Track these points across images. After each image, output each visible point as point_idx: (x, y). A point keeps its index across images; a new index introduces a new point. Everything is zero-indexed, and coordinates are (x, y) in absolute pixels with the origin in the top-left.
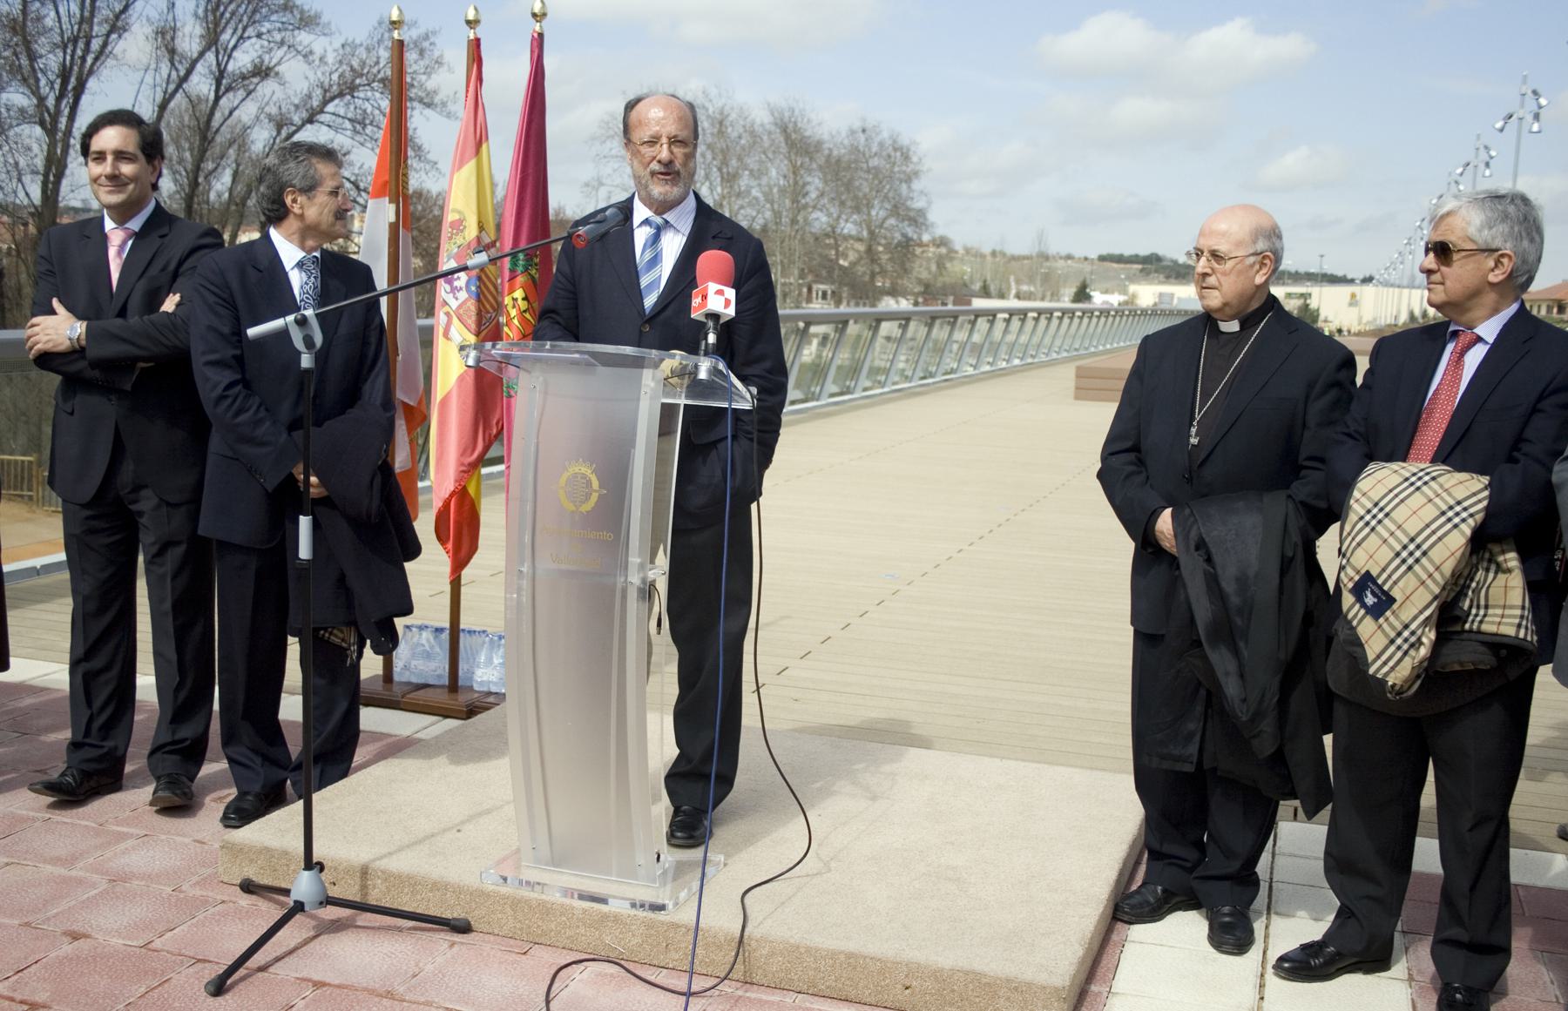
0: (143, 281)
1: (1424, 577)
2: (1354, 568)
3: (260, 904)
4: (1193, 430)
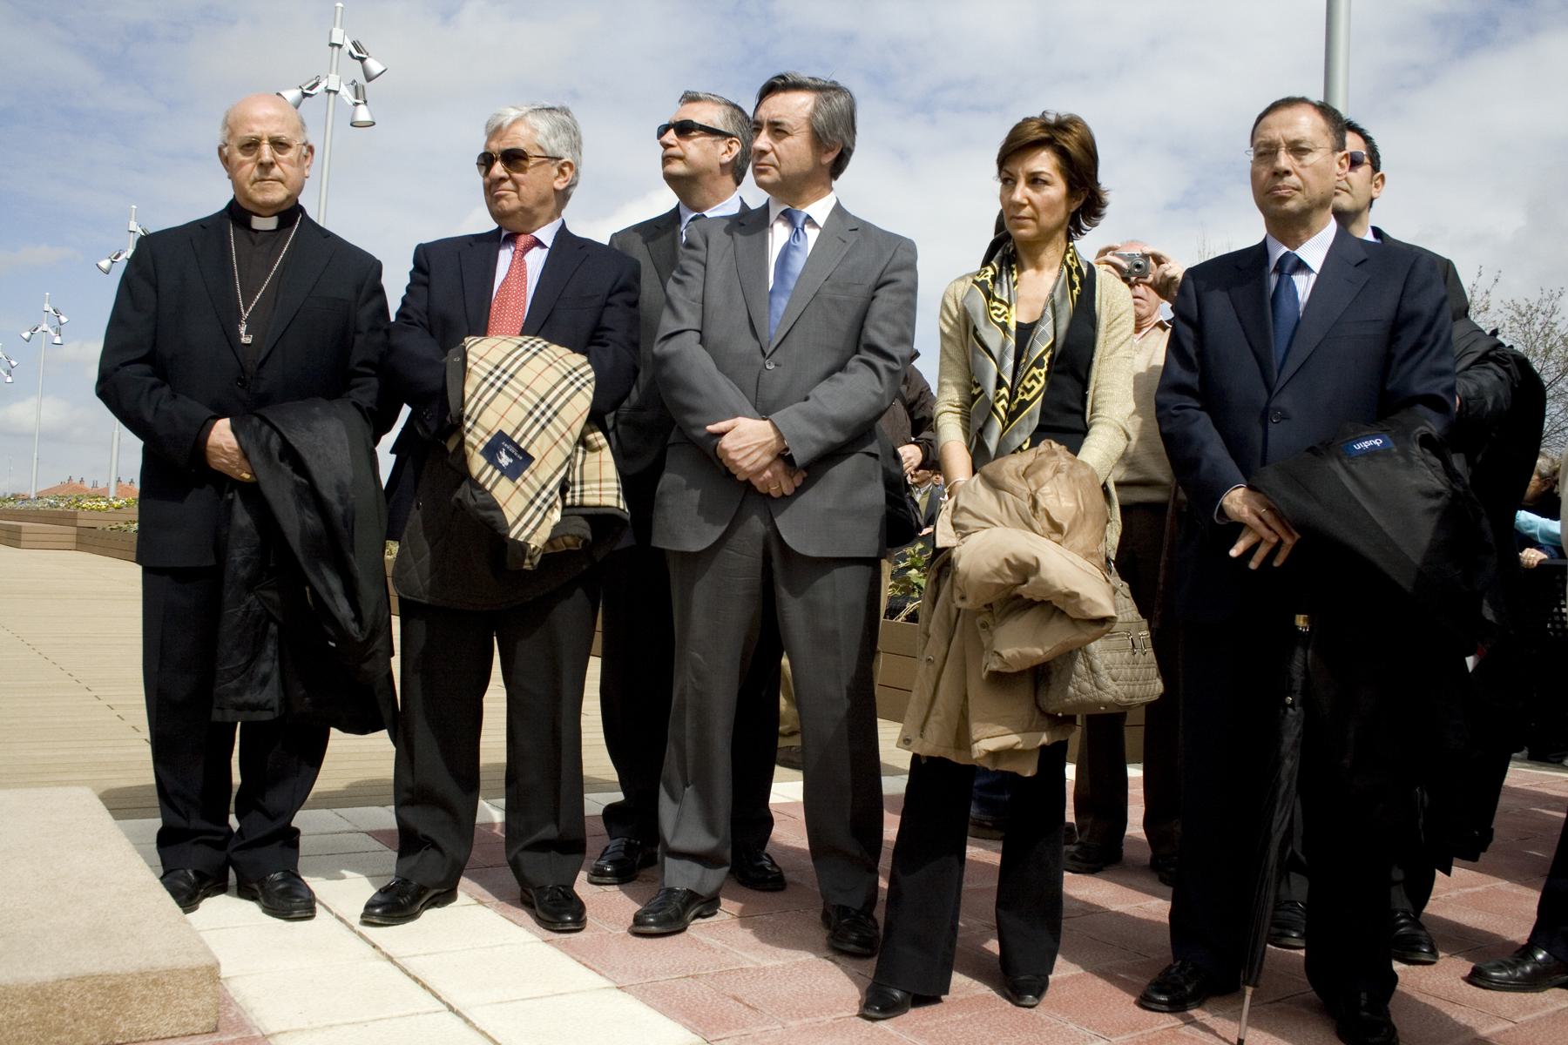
1: (557, 437)
2: (484, 429)
4: (243, 330)
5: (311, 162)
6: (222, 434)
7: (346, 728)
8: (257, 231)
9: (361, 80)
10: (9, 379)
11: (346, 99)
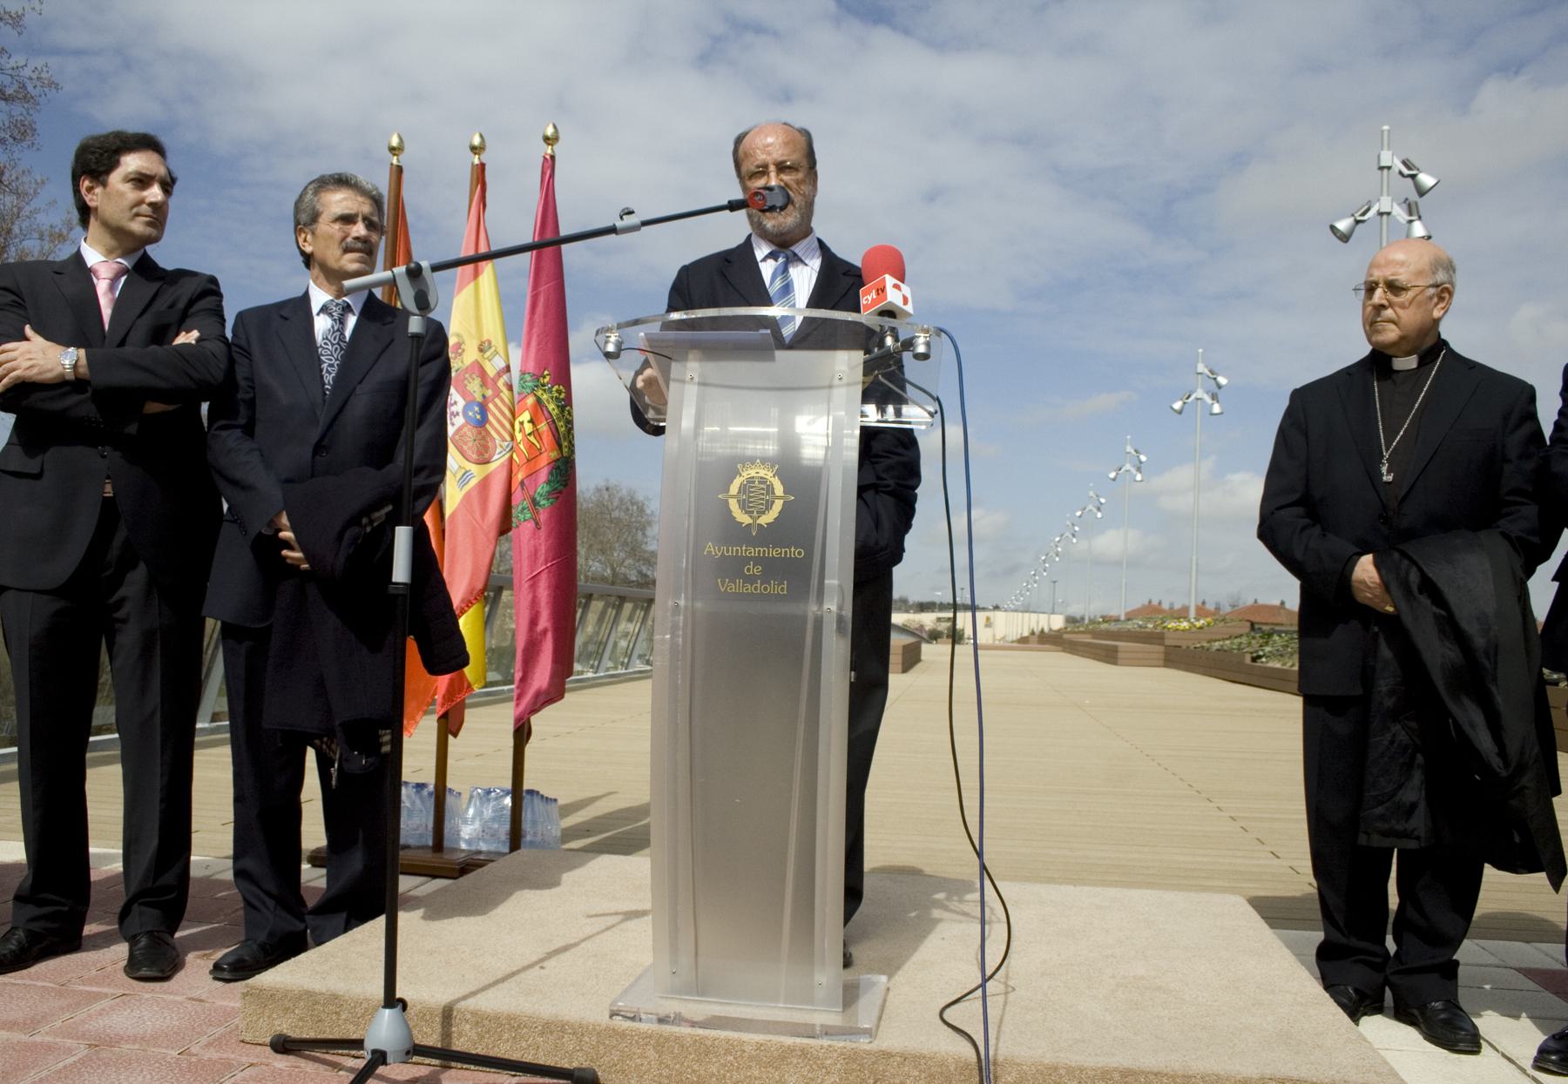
0: (148, 317)
3: (302, 1065)
4: (1384, 469)
6: (1365, 569)
7: (1500, 866)
9: (1414, 196)
10: (1099, 515)
11: (1398, 218)
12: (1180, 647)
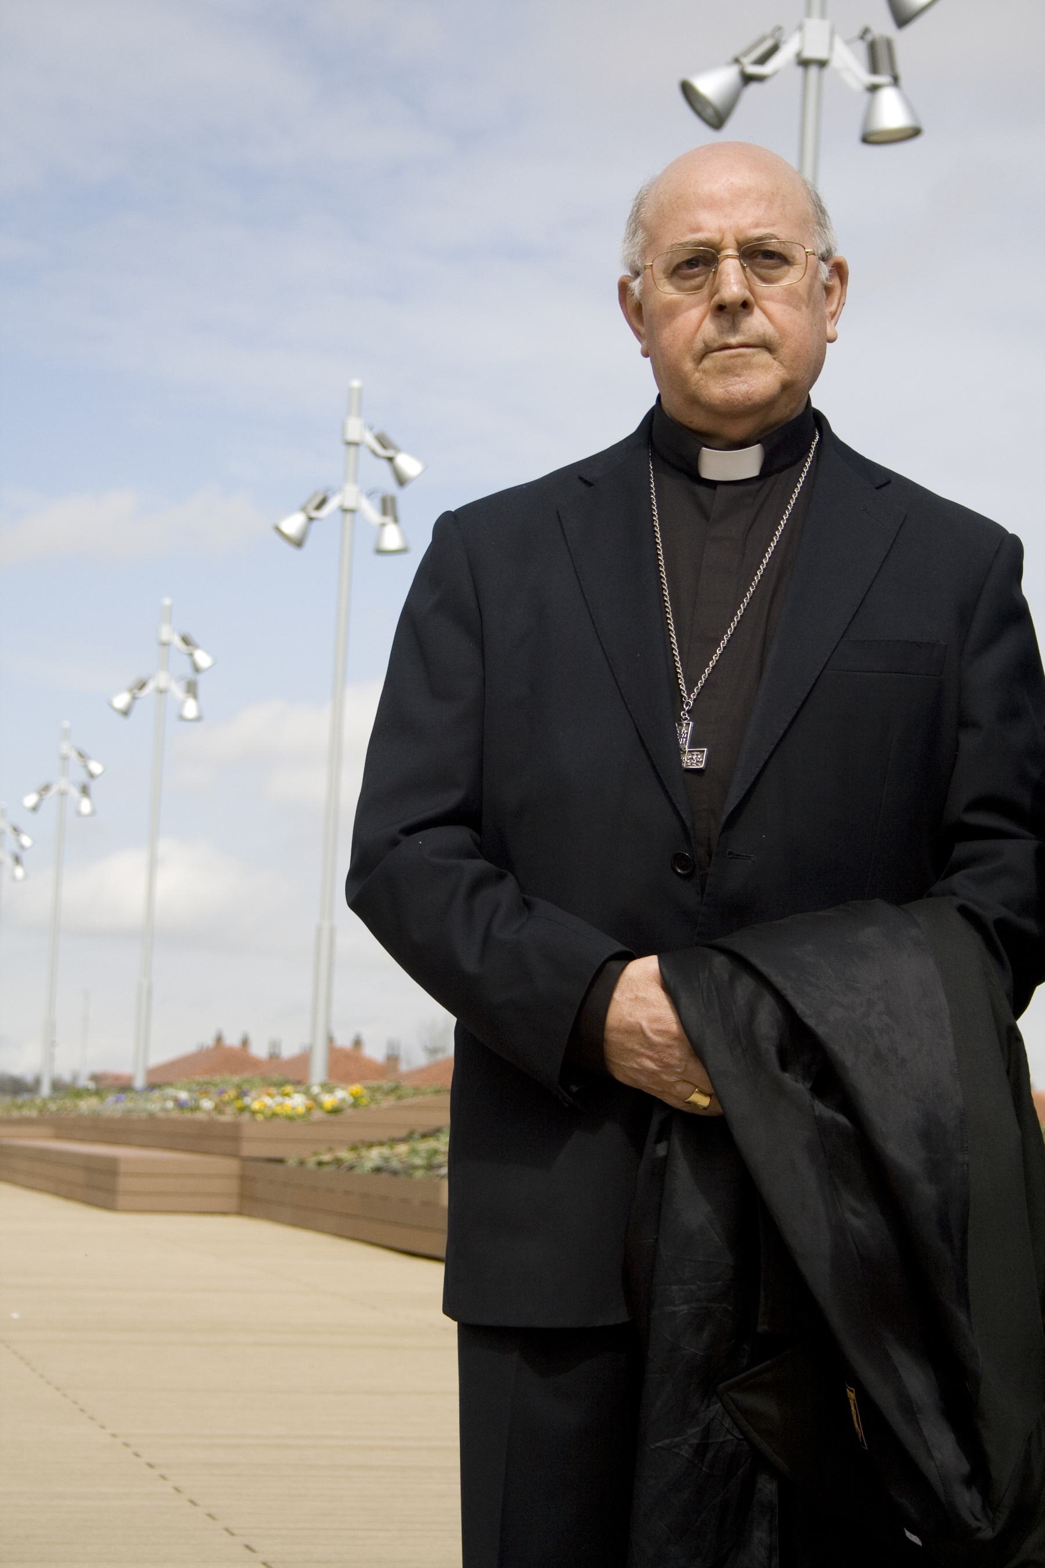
4: (686, 731)
5: (841, 304)
8: (713, 484)
12: (280, 1161)
